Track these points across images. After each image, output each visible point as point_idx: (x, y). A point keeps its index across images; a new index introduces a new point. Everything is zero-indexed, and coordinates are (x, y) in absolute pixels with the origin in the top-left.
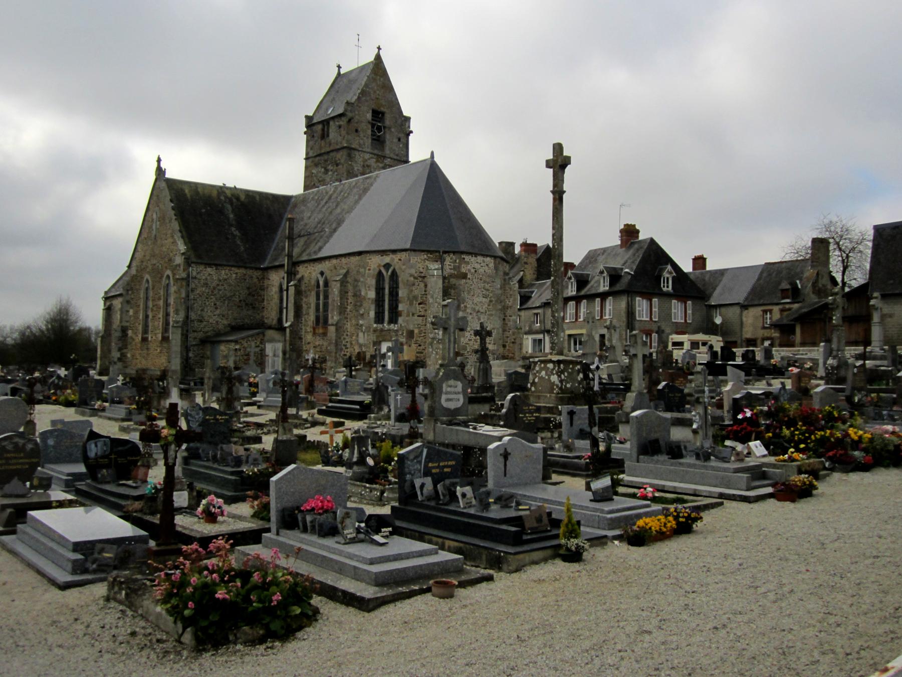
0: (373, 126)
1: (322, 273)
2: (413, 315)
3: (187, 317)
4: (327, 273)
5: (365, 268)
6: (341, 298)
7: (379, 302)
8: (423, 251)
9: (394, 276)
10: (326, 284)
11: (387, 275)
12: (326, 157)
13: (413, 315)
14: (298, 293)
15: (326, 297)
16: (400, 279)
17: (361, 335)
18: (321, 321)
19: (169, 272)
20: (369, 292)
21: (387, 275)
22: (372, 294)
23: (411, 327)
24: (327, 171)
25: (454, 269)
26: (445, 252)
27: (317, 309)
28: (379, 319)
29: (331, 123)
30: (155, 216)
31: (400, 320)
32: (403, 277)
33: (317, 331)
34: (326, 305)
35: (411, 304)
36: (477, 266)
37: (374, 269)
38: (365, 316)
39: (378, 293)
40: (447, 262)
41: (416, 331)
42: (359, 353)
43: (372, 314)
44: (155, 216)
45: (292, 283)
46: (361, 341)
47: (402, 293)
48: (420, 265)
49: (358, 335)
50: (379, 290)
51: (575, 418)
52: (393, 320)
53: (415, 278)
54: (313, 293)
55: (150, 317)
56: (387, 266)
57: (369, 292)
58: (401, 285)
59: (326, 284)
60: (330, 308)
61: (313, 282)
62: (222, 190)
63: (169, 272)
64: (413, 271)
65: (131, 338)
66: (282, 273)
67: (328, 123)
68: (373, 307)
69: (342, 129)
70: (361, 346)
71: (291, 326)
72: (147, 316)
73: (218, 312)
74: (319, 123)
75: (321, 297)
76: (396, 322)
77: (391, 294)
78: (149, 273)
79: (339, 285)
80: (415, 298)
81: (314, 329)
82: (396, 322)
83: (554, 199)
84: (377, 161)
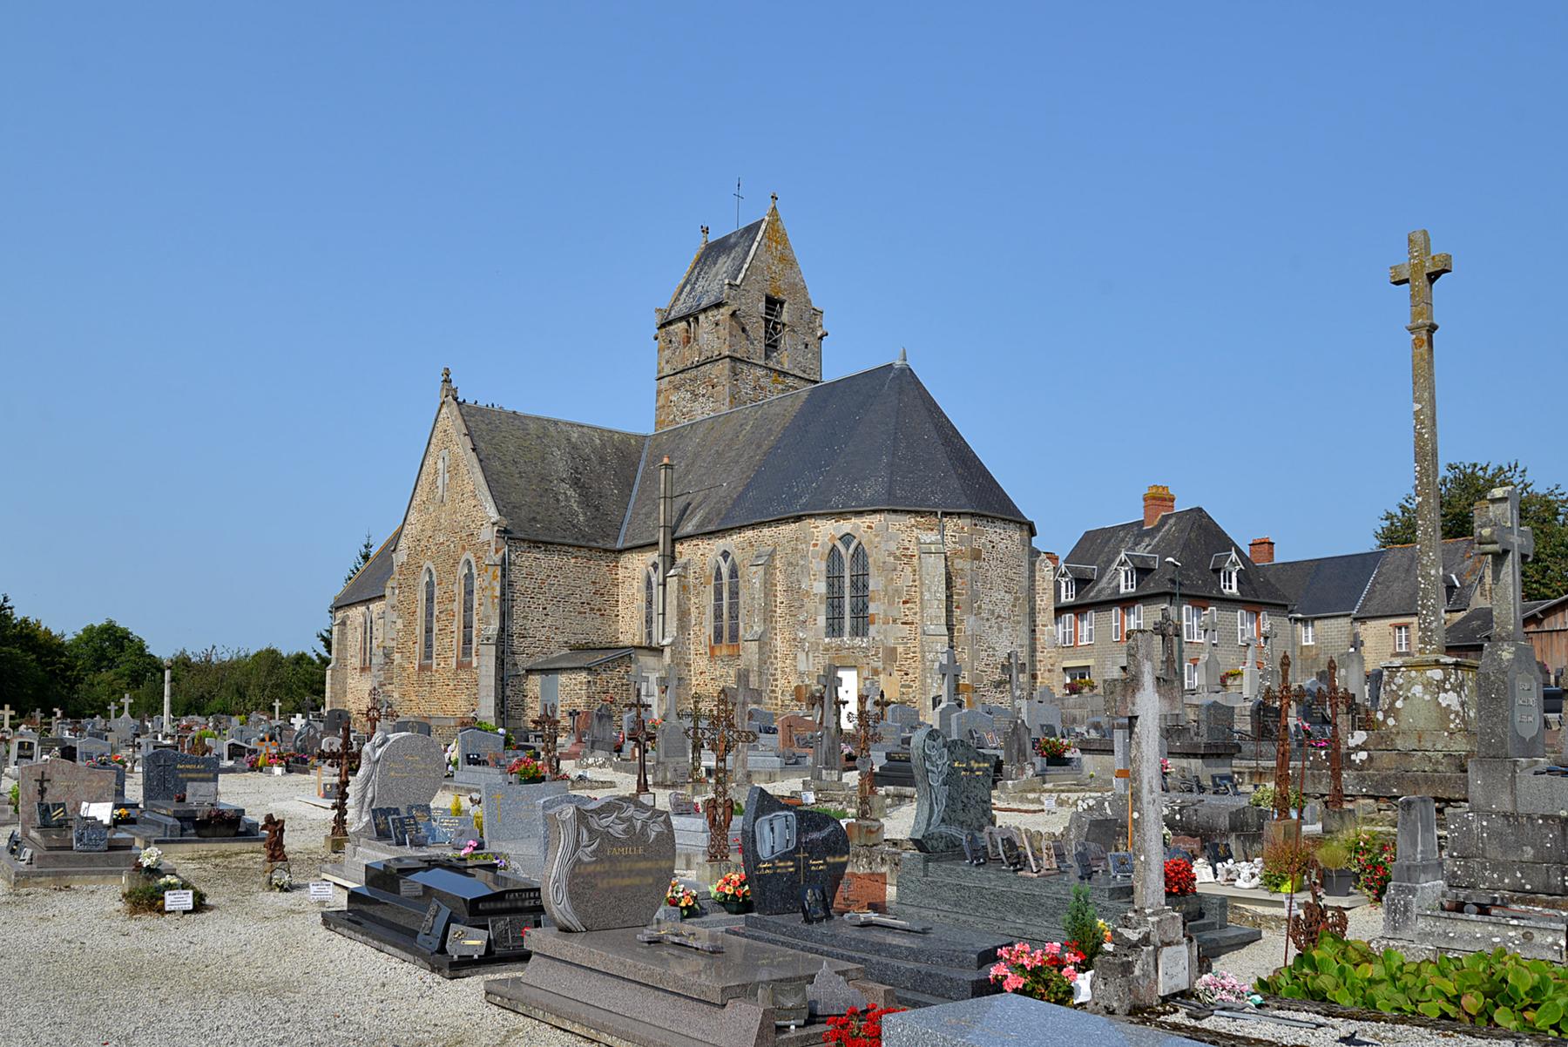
0: (767, 321)
1: (725, 555)
2: (894, 621)
3: (502, 629)
4: (737, 556)
5: (807, 543)
6: (766, 595)
7: (834, 601)
8: (909, 512)
9: (860, 555)
10: (734, 573)
11: (847, 554)
12: (694, 372)
13: (894, 621)
14: (683, 588)
15: (734, 594)
16: (870, 560)
17: (801, 656)
18: (726, 634)
19: (469, 555)
20: (815, 584)
21: (847, 554)
22: (821, 587)
23: (891, 642)
24: (695, 396)
25: (961, 542)
26: (945, 514)
27: (718, 616)
28: (834, 628)
29: (702, 317)
30: (440, 465)
31: (872, 630)
32: (875, 557)
33: (717, 653)
34: (734, 607)
35: (891, 603)
36: (996, 538)
37: (824, 544)
38: (810, 624)
39: (830, 586)
40: (948, 532)
41: (900, 649)
42: (798, 688)
43: (822, 621)
44: (440, 465)
45: (672, 572)
46: (802, 667)
47: (875, 583)
48: (904, 536)
49: (795, 658)
50: (834, 579)
51: (436, 945)
52: (860, 629)
53: (896, 558)
54: (710, 589)
55: (435, 630)
56: (847, 538)
57: (815, 584)
58: (872, 570)
59: (734, 573)
60: (742, 612)
61: (710, 571)
62: (546, 426)
63: (469, 555)
64: (893, 546)
65: (400, 665)
66: (653, 556)
67: (697, 319)
68: (823, 608)
69: (721, 328)
70: (801, 674)
71: (672, 644)
72: (429, 630)
73: (549, 621)
74: (681, 319)
75: (725, 595)
76: (865, 634)
77: (854, 585)
78: (431, 558)
79: (762, 572)
80: (897, 591)
81: (712, 649)
82: (865, 634)
83: (1417, 344)
84: (775, 382)
